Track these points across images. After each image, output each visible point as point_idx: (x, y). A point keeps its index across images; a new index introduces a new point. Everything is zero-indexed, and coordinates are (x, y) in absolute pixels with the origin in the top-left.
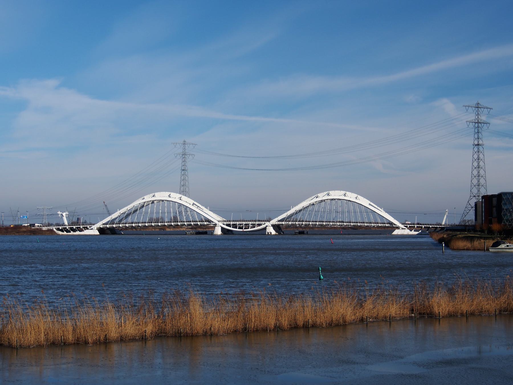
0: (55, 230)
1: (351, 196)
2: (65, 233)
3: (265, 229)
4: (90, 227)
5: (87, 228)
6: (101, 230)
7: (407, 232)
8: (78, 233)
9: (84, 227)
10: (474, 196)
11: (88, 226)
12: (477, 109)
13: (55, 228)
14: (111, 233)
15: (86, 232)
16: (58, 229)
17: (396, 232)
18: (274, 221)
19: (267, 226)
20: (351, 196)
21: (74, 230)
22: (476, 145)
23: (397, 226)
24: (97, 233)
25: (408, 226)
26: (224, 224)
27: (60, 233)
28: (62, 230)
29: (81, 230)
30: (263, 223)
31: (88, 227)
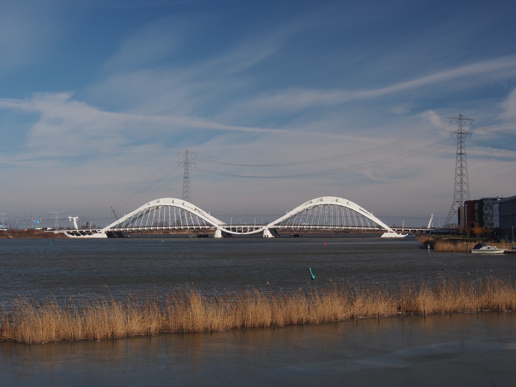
0: (66, 233)
1: (343, 202)
2: (75, 236)
3: (262, 232)
4: (99, 231)
5: (96, 232)
6: (109, 234)
7: (395, 235)
8: (87, 236)
9: (93, 231)
10: (458, 202)
11: (97, 230)
12: (460, 120)
13: (66, 232)
14: (118, 237)
15: (95, 236)
16: (69, 233)
17: (385, 235)
18: (271, 225)
19: (264, 230)
20: (343, 202)
21: (84, 234)
22: (459, 154)
23: (386, 230)
24: (105, 236)
25: (396, 229)
26: (224, 228)
27: (71, 236)
28: (72, 234)
29: (90, 234)
30: (261, 226)
31: (97, 231)
